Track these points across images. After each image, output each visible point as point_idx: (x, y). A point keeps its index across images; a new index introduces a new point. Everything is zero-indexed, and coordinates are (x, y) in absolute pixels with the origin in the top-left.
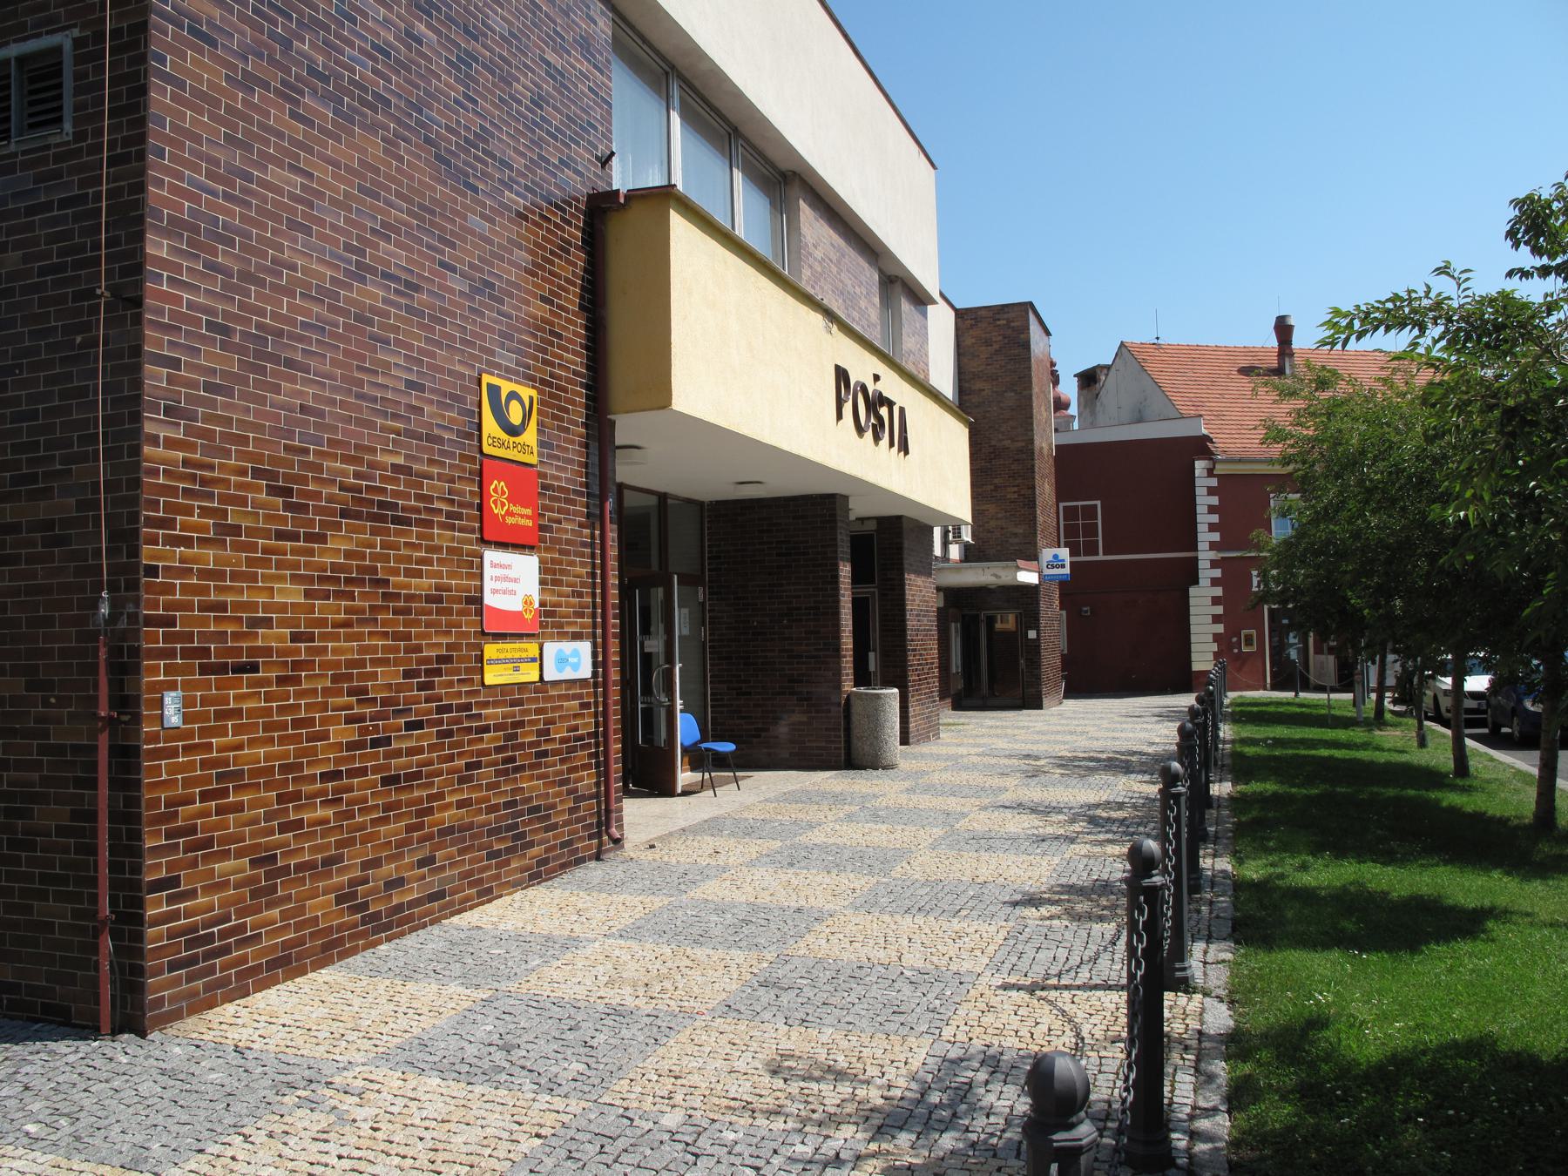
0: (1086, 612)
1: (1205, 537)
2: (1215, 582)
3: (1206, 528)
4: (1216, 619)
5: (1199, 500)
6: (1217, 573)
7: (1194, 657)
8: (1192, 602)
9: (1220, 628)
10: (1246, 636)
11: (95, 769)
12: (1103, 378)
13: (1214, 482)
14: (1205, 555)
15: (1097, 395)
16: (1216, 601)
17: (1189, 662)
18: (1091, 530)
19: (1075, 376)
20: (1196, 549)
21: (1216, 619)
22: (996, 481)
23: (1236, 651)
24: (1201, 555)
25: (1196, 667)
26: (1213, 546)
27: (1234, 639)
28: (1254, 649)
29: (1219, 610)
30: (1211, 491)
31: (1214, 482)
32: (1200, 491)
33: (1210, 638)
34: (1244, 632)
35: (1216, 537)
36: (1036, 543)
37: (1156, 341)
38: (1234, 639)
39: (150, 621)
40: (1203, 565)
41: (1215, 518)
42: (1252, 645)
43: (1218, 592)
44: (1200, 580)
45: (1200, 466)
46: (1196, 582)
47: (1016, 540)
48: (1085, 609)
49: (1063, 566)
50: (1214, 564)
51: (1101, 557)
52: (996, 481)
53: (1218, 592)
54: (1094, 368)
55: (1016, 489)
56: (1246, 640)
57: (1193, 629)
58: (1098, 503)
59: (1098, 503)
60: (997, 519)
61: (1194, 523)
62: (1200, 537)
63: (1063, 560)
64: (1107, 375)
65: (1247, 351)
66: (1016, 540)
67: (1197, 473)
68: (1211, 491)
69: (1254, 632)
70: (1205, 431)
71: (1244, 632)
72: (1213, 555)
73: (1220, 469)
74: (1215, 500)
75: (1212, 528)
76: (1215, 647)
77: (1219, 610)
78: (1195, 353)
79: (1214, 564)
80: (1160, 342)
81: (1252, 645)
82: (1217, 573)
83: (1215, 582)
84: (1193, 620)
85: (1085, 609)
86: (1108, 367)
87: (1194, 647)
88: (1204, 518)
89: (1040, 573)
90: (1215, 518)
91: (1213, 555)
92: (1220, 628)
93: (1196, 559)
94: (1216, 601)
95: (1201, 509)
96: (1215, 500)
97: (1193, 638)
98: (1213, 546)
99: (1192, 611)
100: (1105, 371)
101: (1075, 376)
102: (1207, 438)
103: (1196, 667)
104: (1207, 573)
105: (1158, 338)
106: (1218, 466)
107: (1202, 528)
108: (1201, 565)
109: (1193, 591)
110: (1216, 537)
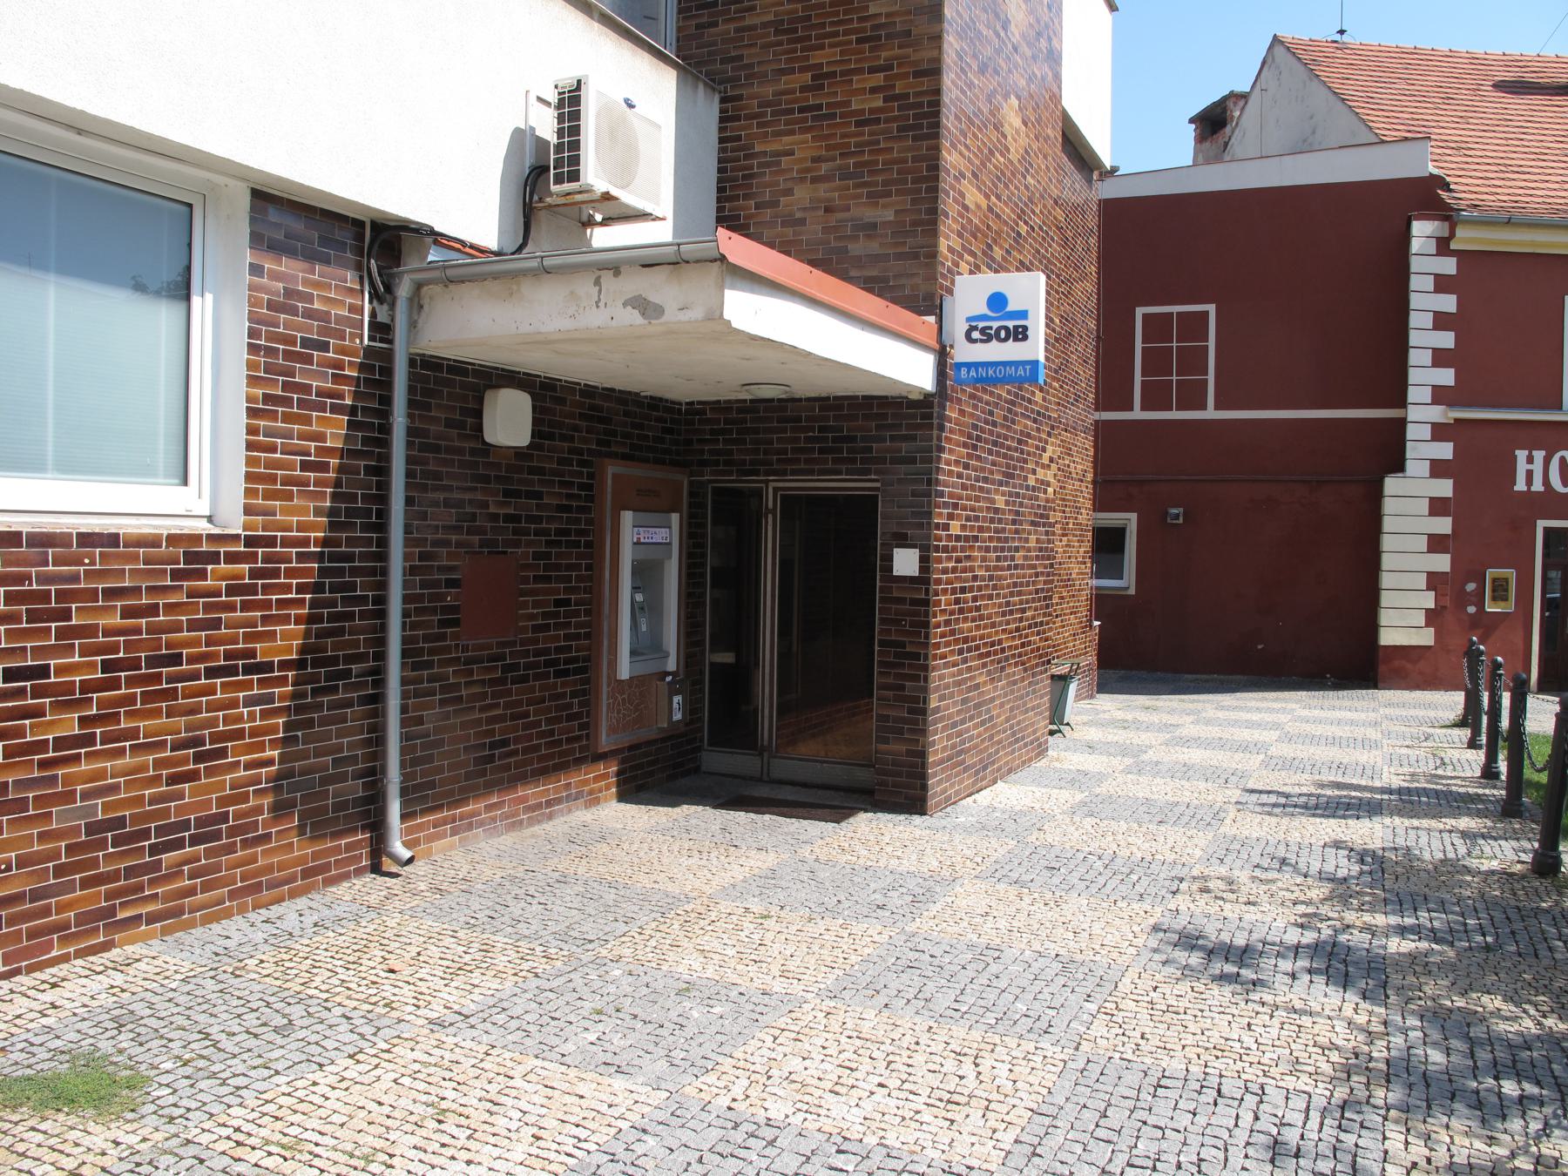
0: (1177, 517)
1: (1424, 376)
2: (1438, 469)
3: (1427, 357)
4: (1436, 543)
5: (1415, 301)
6: (1445, 451)
7: (1385, 618)
8: (1389, 506)
9: (1442, 562)
10: (1494, 580)
11: (405, 640)
12: (1237, 114)
13: (1449, 266)
14: (1421, 414)
15: (1226, 144)
16: (1438, 507)
17: (1373, 627)
18: (1193, 362)
19: (1191, 121)
20: (1402, 403)
21: (1436, 543)
22: (818, 57)
23: (1472, 609)
24: (1413, 413)
25: (1388, 638)
26: (1440, 395)
27: (1471, 587)
28: (1509, 607)
29: (1444, 525)
30: (1442, 284)
31: (1449, 266)
32: (1420, 283)
33: (1422, 582)
34: (1490, 573)
35: (1447, 377)
36: (933, 255)
37: (1338, 37)
38: (1471, 587)
39: (937, 549)
40: (1416, 432)
41: (1447, 340)
42: (1505, 599)
43: (1445, 488)
44: (1408, 463)
45: (1423, 231)
46: (1398, 466)
47: (874, 247)
48: (1175, 511)
49: (1020, 334)
50: (1440, 432)
51: (1210, 413)
52: (818, 57)
53: (1445, 488)
54: (1224, 100)
55: (879, 79)
56: (1494, 590)
57: (1387, 561)
58: (1211, 309)
59: (1211, 309)
60: (815, 180)
61: (1402, 347)
62: (1414, 376)
63: (1023, 314)
64: (1243, 109)
65: (1508, 61)
66: (874, 247)
67: (1416, 245)
68: (1442, 284)
69: (1511, 574)
70: (1432, 169)
71: (1490, 573)
72: (1438, 414)
73: (1465, 239)
74: (1448, 303)
75: (1440, 358)
76: (1429, 600)
77: (1444, 525)
78: (1413, 60)
79: (1440, 432)
80: (1346, 38)
81: (1505, 599)
82: (1445, 451)
83: (1438, 469)
84: (1387, 543)
85: (1175, 511)
86: (1244, 97)
87: (1386, 599)
88: (1424, 338)
89: (942, 354)
90: (1447, 340)
91: (1438, 414)
92: (1442, 562)
93: (1402, 423)
94: (1438, 507)
95: (1419, 321)
96: (1448, 303)
97: (1386, 580)
98: (1440, 395)
99: (1388, 524)
100: (1241, 103)
101: (1191, 121)
102: (1440, 182)
103: (1388, 638)
104: (1422, 449)
105: (1342, 32)
106: (1461, 232)
107: (1418, 358)
108: (1412, 432)
109: (1391, 484)
110: (1447, 377)
